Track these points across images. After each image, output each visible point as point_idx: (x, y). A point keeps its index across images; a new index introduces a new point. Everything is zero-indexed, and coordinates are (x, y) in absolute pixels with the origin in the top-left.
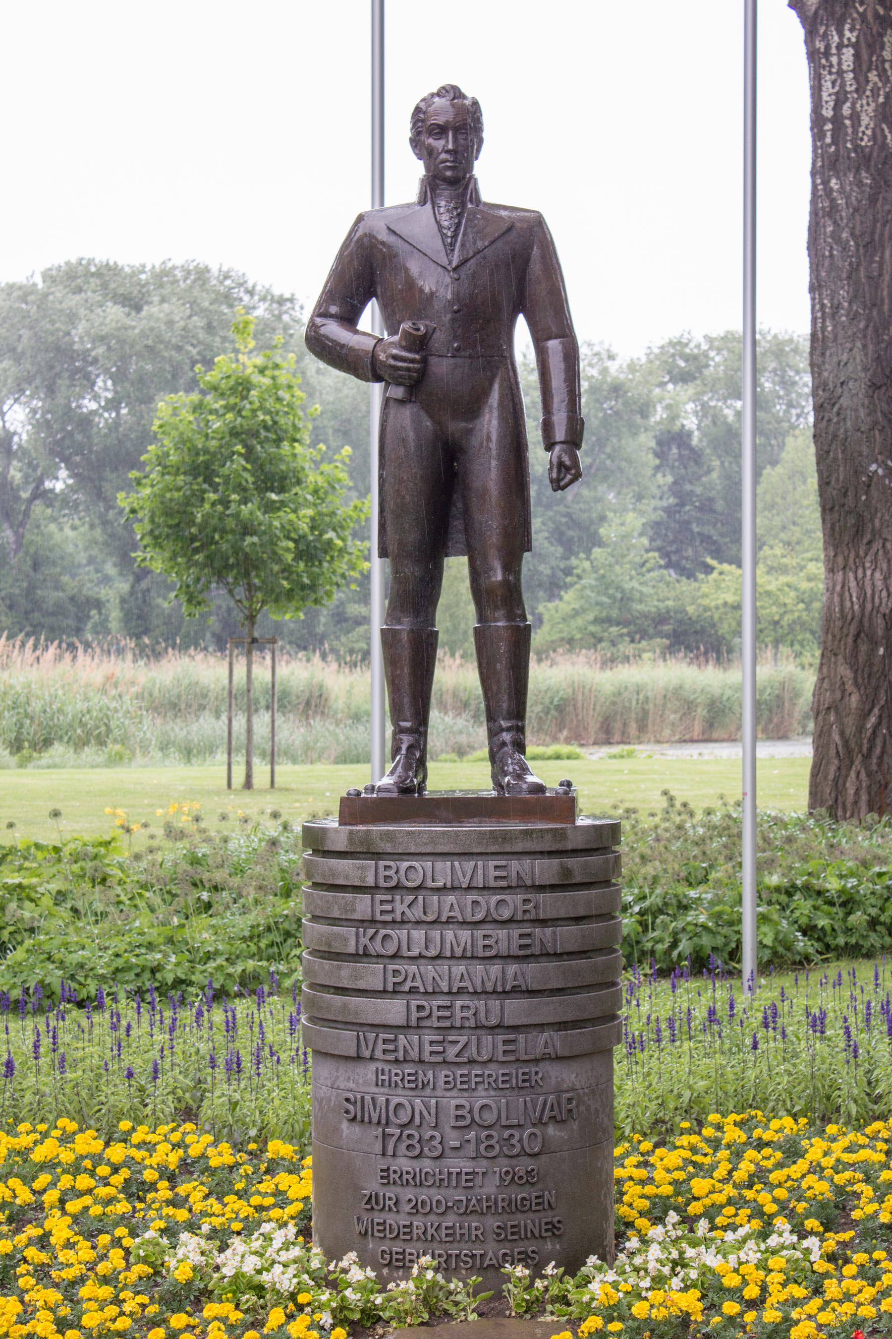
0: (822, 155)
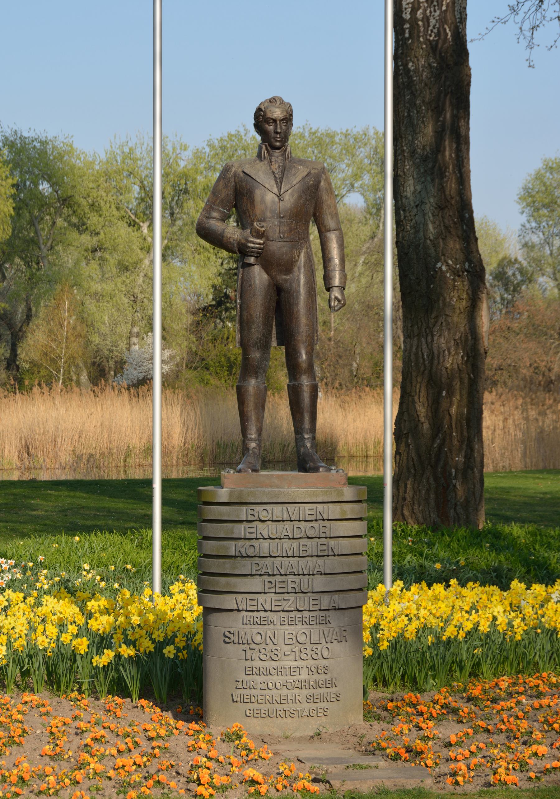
0: (402, 45)
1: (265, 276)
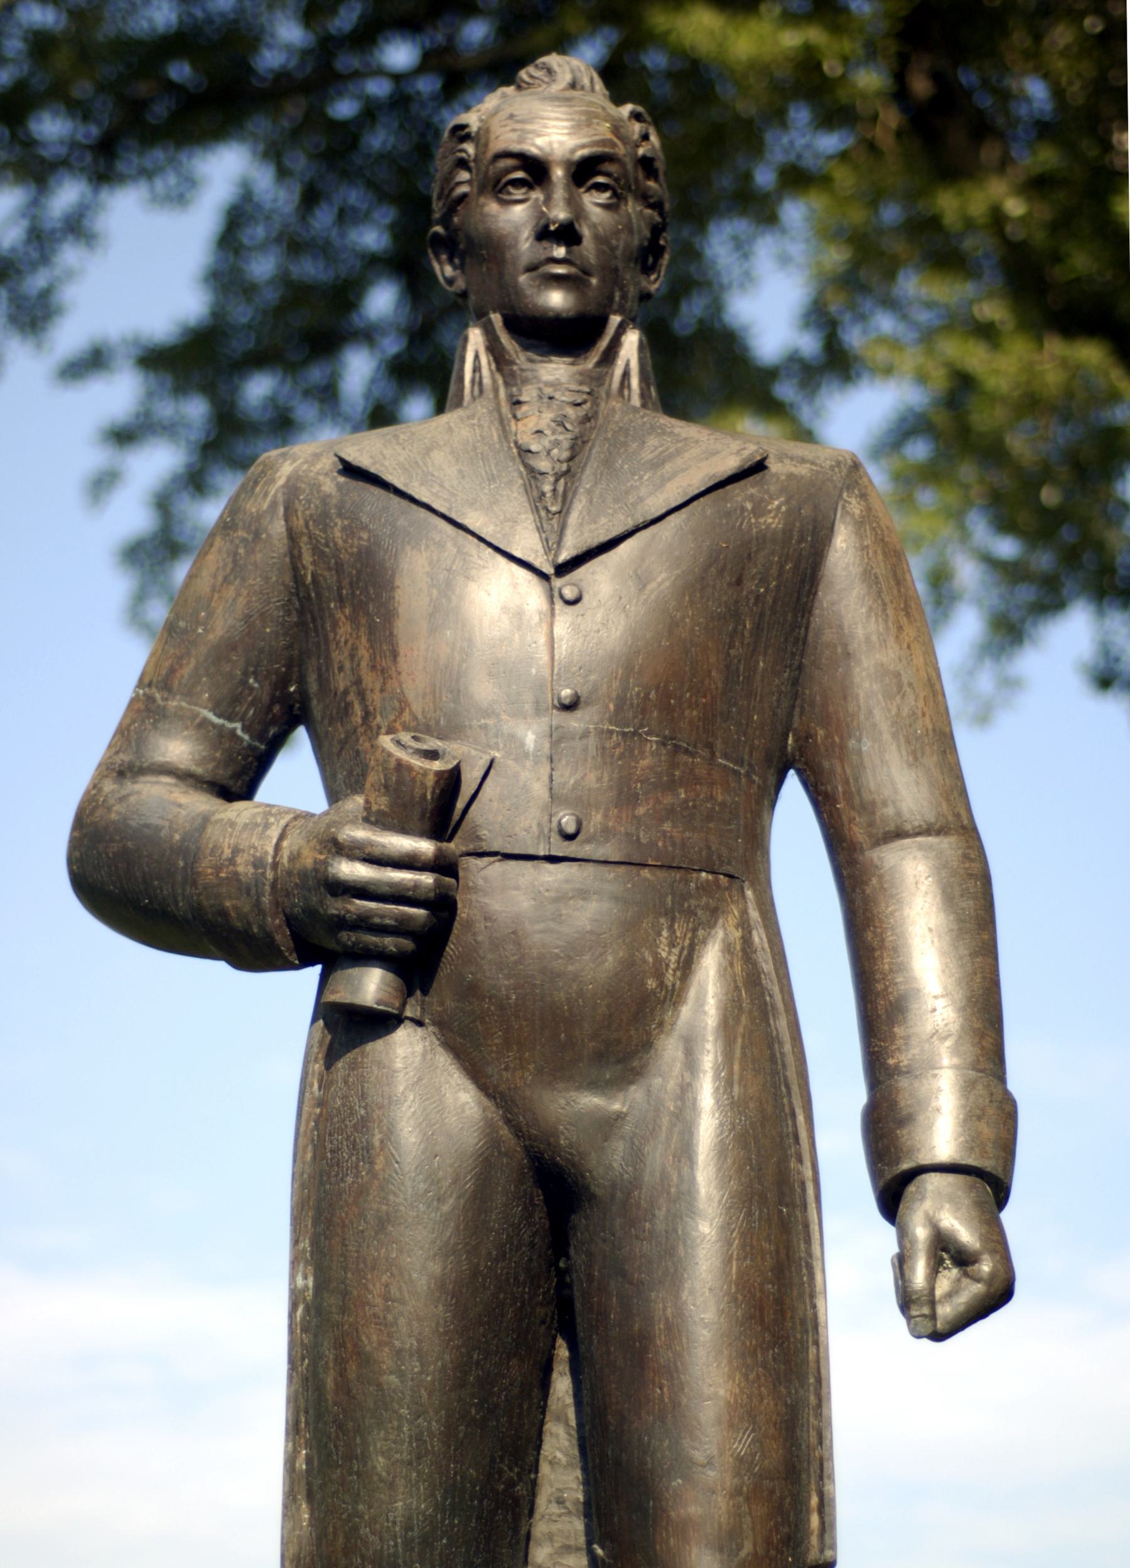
1: (462, 1100)
